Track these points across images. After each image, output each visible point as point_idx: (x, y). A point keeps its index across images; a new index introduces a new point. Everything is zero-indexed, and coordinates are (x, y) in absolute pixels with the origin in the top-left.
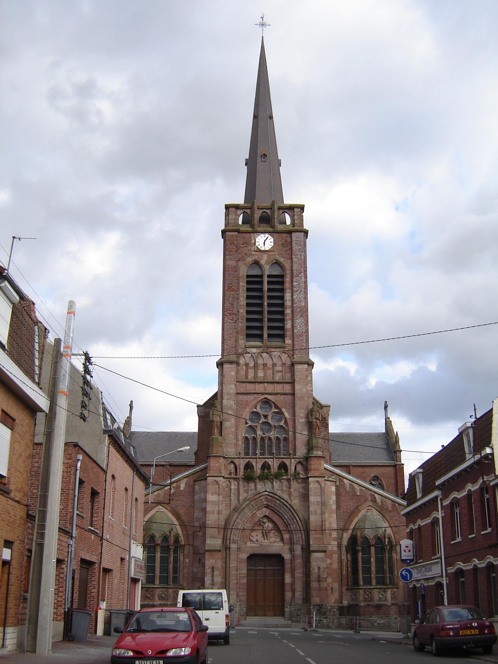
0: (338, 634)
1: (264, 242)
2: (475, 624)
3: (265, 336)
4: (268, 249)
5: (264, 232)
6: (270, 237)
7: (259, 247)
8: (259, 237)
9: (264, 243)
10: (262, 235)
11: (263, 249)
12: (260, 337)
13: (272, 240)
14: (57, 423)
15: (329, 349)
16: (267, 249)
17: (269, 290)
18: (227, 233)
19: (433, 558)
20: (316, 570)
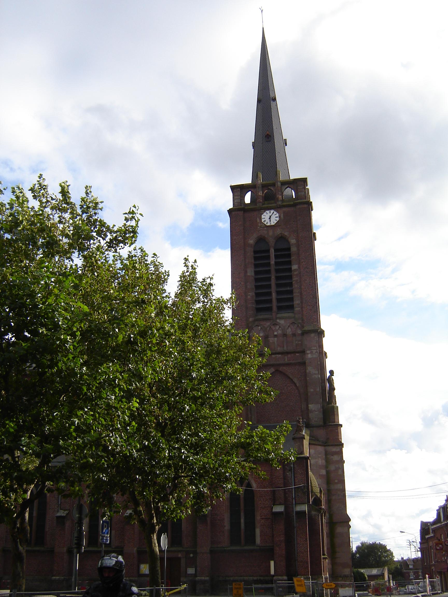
0: (359, 583)
1: (270, 218)
2: (30, 367)
3: (275, 308)
4: (274, 224)
5: (269, 209)
6: (275, 213)
7: (265, 223)
8: (265, 214)
9: (270, 218)
10: (268, 212)
11: (269, 224)
12: (269, 309)
13: (277, 215)
14: (256, 534)
15: (354, 533)
16: (273, 224)
17: (276, 263)
18: (233, 213)
19: (391, 576)
20: (328, 374)
